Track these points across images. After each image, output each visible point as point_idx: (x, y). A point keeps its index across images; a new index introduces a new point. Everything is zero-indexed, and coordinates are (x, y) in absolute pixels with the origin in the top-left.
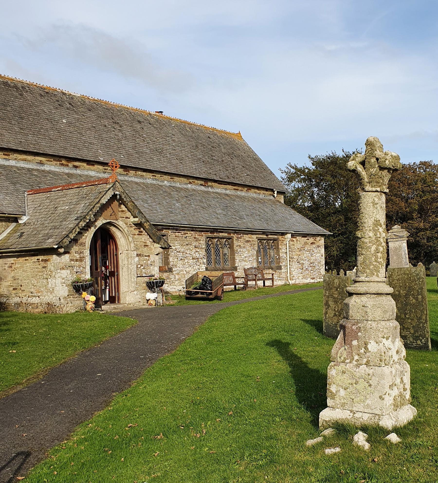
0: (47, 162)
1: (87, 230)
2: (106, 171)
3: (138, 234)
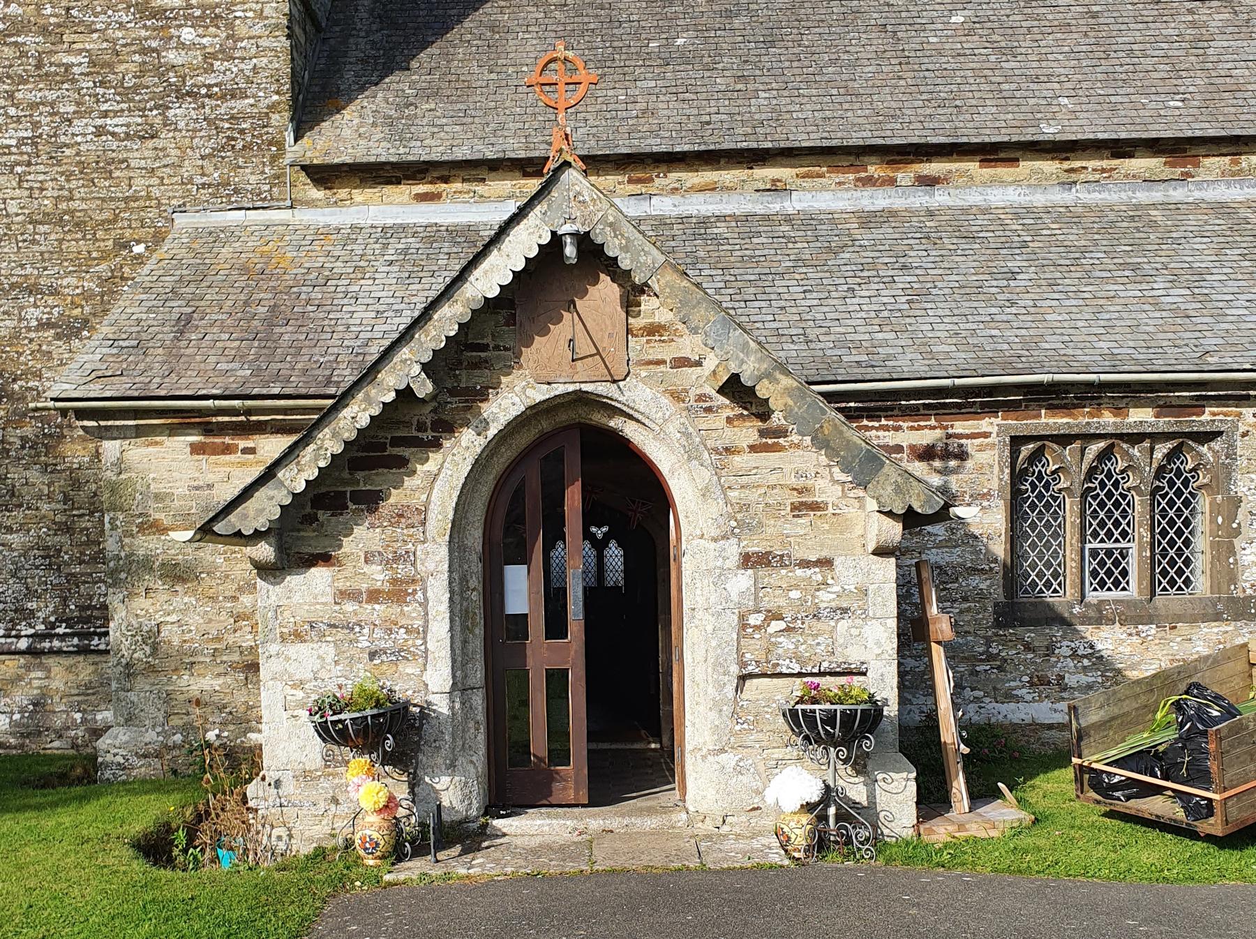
0: (799, 181)
1: (436, 445)
2: (1074, 176)
3: (753, 448)
